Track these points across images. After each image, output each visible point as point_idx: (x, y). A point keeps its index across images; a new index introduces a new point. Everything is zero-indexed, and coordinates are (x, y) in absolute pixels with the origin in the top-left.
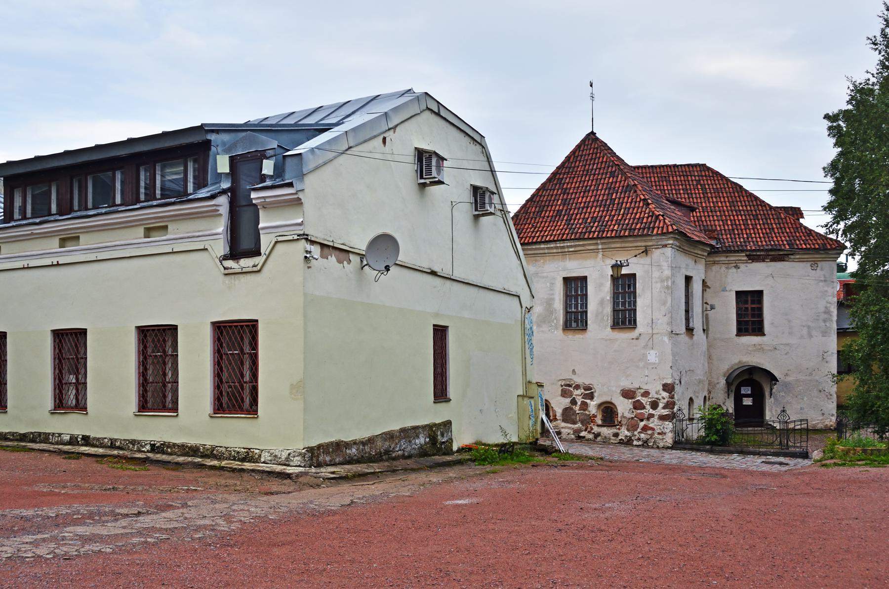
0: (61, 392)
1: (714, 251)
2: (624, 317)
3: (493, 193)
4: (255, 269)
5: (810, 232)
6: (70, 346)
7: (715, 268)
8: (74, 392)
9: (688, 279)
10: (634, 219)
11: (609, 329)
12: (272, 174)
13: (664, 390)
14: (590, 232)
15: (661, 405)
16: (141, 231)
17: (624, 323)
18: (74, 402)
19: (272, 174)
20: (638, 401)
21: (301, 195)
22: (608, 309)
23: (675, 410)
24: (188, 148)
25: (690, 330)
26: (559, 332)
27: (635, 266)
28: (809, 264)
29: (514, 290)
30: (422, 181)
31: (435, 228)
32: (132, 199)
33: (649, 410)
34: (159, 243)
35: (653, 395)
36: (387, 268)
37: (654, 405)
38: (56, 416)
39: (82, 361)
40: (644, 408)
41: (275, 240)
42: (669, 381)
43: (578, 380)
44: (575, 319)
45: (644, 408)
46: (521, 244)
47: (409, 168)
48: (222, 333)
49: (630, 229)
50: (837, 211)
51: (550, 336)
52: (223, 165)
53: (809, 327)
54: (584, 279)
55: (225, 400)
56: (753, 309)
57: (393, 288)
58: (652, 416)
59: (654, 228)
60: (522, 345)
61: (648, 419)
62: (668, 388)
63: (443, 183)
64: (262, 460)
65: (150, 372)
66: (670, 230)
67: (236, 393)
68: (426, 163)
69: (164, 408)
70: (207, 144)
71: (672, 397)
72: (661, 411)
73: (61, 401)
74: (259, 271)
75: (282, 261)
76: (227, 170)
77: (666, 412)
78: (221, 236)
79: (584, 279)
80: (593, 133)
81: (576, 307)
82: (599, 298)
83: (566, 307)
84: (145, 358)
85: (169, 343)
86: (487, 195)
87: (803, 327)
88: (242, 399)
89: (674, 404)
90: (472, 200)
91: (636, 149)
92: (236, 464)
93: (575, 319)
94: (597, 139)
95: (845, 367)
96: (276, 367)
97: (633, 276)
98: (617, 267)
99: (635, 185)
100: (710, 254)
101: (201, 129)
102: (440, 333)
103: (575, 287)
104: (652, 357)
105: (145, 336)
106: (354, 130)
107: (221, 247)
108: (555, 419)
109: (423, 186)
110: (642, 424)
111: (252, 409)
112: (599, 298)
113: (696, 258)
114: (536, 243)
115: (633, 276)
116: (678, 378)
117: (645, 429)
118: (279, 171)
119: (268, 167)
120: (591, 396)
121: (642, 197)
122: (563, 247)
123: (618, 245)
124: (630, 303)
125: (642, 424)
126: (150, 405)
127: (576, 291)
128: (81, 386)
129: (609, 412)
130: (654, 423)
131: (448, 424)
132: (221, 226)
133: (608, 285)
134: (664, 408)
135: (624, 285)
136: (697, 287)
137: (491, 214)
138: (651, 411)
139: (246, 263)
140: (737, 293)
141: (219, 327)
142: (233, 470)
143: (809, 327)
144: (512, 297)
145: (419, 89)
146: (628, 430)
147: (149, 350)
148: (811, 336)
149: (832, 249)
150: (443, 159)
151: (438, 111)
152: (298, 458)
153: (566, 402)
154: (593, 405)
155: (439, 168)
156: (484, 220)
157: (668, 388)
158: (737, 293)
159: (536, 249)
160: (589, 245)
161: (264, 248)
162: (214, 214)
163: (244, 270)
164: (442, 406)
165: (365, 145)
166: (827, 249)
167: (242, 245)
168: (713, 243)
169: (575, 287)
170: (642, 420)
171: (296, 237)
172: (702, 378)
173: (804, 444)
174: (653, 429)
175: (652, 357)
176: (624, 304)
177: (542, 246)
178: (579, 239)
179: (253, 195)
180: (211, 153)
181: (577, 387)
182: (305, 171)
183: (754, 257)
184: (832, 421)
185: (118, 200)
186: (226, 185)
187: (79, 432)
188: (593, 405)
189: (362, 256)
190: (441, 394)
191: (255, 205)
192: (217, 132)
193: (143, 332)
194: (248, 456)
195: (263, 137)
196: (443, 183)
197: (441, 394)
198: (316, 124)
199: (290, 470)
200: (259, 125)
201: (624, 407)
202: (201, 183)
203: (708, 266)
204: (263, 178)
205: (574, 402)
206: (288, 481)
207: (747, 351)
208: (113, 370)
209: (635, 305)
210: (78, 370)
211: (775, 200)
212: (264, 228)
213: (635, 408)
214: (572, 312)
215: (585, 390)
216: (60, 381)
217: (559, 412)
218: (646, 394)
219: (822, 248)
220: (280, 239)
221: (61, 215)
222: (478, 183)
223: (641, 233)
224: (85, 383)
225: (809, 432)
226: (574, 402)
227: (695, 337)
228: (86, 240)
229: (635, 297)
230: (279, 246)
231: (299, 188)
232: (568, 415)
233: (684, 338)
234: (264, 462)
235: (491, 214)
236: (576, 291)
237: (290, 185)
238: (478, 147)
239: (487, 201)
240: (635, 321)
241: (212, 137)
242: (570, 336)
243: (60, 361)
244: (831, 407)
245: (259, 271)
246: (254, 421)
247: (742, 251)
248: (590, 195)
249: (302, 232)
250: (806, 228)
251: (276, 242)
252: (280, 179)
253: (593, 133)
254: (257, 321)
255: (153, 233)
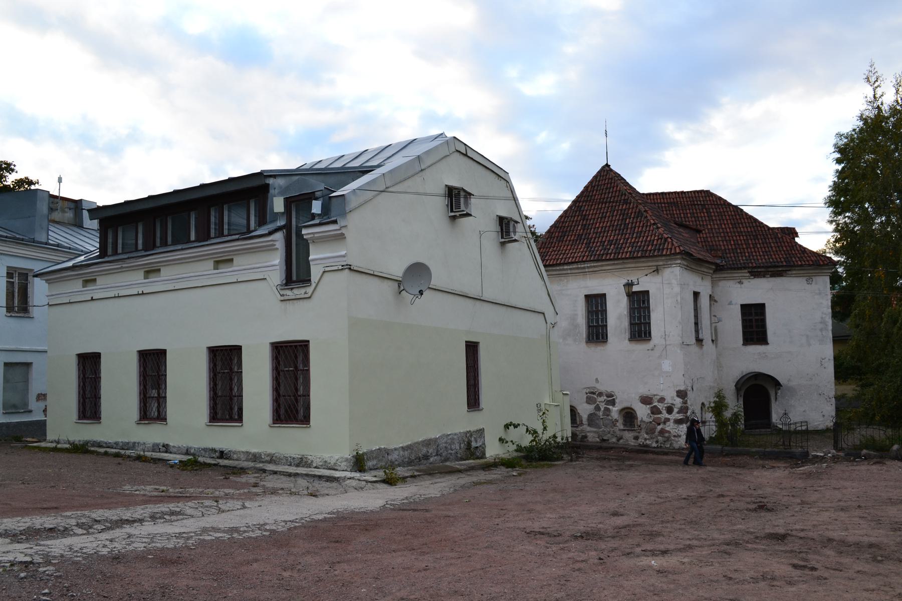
0: (145, 405)
1: (719, 269)
2: (640, 329)
3: (517, 222)
4: (306, 296)
5: (804, 250)
6: (152, 363)
7: (722, 284)
8: (156, 405)
9: (696, 295)
10: (646, 241)
11: (627, 341)
12: (319, 212)
13: (678, 396)
14: (607, 254)
15: (676, 410)
16: (210, 264)
17: (640, 336)
18: (156, 414)
19: (319, 212)
20: (655, 406)
21: (343, 231)
22: (626, 323)
23: (689, 413)
24: (250, 191)
25: (699, 341)
26: (583, 344)
27: (645, 282)
28: (804, 279)
29: (539, 309)
30: (453, 214)
31: (464, 256)
32: (204, 236)
33: (665, 415)
34: (227, 274)
35: (669, 400)
36: (421, 292)
37: (670, 410)
38: (141, 426)
39: (163, 378)
40: (661, 413)
41: (323, 270)
42: (682, 388)
43: (602, 388)
44: (597, 333)
45: (661, 413)
46: (545, 266)
47: (441, 203)
48: (279, 353)
49: (659, 249)
50: (874, 224)
51: (577, 349)
52: (278, 205)
53: (807, 336)
54: (603, 296)
55: (282, 411)
56: (757, 320)
57: (429, 310)
58: (668, 420)
59: (663, 249)
60: (550, 359)
61: (665, 423)
62: (682, 394)
63: (471, 215)
64: (315, 465)
65: (219, 387)
66: (678, 251)
67: (291, 407)
68: (456, 200)
69: (231, 419)
70: (266, 187)
71: (685, 403)
72: (675, 415)
73: (145, 413)
74: (309, 298)
75: (330, 291)
76: (282, 210)
77: (680, 416)
78: (278, 267)
79: (603, 296)
80: (607, 165)
81: (597, 321)
82: (617, 312)
83: (588, 322)
84: (215, 375)
85: (300, 359)
86: (512, 224)
87: (802, 336)
88: (297, 411)
89: (687, 409)
90: (499, 229)
91: (647, 181)
92: (292, 470)
93: (597, 333)
94: (611, 170)
95: (842, 372)
96: (327, 383)
97: (647, 293)
98: (629, 285)
99: (646, 211)
100: (715, 271)
101: (261, 175)
102: (472, 349)
103: (596, 304)
104: (666, 366)
105: (215, 356)
106: (391, 172)
107: (277, 276)
108: (582, 424)
109: (454, 218)
110: (659, 427)
111: (305, 420)
112: (617, 312)
113: (703, 275)
114: (560, 264)
115: (647, 293)
116: (690, 385)
117: (662, 432)
118: (326, 209)
119: (316, 207)
120: (613, 403)
121: (652, 222)
122: (584, 268)
123: (633, 265)
124: (645, 317)
125: (659, 427)
126: (219, 416)
127: (597, 307)
128: (161, 399)
129: (629, 415)
130: (670, 427)
131: (481, 432)
132: (277, 259)
133: (625, 300)
134: (678, 413)
135: (639, 303)
136: (704, 301)
137: (515, 241)
138: (667, 416)
139: (299, 292)
140: (742, 306)
141: (276, 348)
142: (290, 475)
143: (807, 336)
144: (537, 314)
145: (450, 134)
146: (647, 433)
147: (218, 368)
148: (809, 345)
149: (824, 265)
150: (470, 194)
151: (465, 153)
152: (344, 463)
153: (590, 408)
154: (615, 410)
155: (467, 204)
156: (510, 246)
157: (682, 394)
158: (742, 306)
159: (560, 270)
160: (607, 266)
161: (314, 277)
162: (271, 248)
163: (298, 297)
164: (475, 415)
165: (400, 184)
166: (820, 265)
167: (296, 275)
168: (718, 261)
169: (596, 304)
170: (659, 424)
171: (340, 267)
172: (712, 384)
173: (804, 444)
174: (669, 432)
175: (666, 366)
176: (639, 318)
177: (566, 267)
178: (598, 261)
179: (304, 232)
180: (269, 195)
181: (600, 394)
182: (348, 209)
183: (757, 273)
184: (830, 424)
185: (193, 238)
186: (281, 222)
187: (160, 440)
188: (615, 410)
189: (399, 283)
190: (473, 402)
191: (306, 240)
192: (274, 176)
193: (214, 352)
194: (302, 462)
195: (312, 180)
196: (471, 215)
197: (473, 402)
198: (360, 166)
199: (337, 474)
200: (311, 169)
201: (643, 412)
202: (262, 222)
203: (714, 284)
204: (313, 216)
205: (598, 408)
206: (334, 484)
207: (753, 359)
208: (188, 384)
209: (649, 319)
210: (159, 385)
211: (772, 220)
212: (313, 260)
213: (653, 413)
214: (594, 326)
215: (608, 396)
216: (145, 396)
217: (585, 417)
218: (662, 400)
219: (814, 262)
220: (327, 269)
221: (146, 251)
222: (503, 214)
223: (652, 254)
224: (165, 397)
225: (808, 434)
226: (598, 408)
227: (705, 348)
228: (165, 272)
229: (649, 312)
230: (326, 274)
231: (343, 224)
232: (592, 418)
233: (695, 349)
234: (316, 467)
235: (515, 241)
236: (597, 307)
237: (335, 222)
238: (503, 182)
239: (511, 230)
240: (650, 333)
241: (271, 181)
242: (593, 349)
243: (145, 378)
244: (830, 409)
245: (309, 298)
246: (307, 430)
247: (745, 268)
248: (612, 221)
249: (344, 263)
250: (800, 246)
251: (324, 272)
252: (327, 217)
253: (607, 165)
254: (308, 341)
255: (221, 266)
